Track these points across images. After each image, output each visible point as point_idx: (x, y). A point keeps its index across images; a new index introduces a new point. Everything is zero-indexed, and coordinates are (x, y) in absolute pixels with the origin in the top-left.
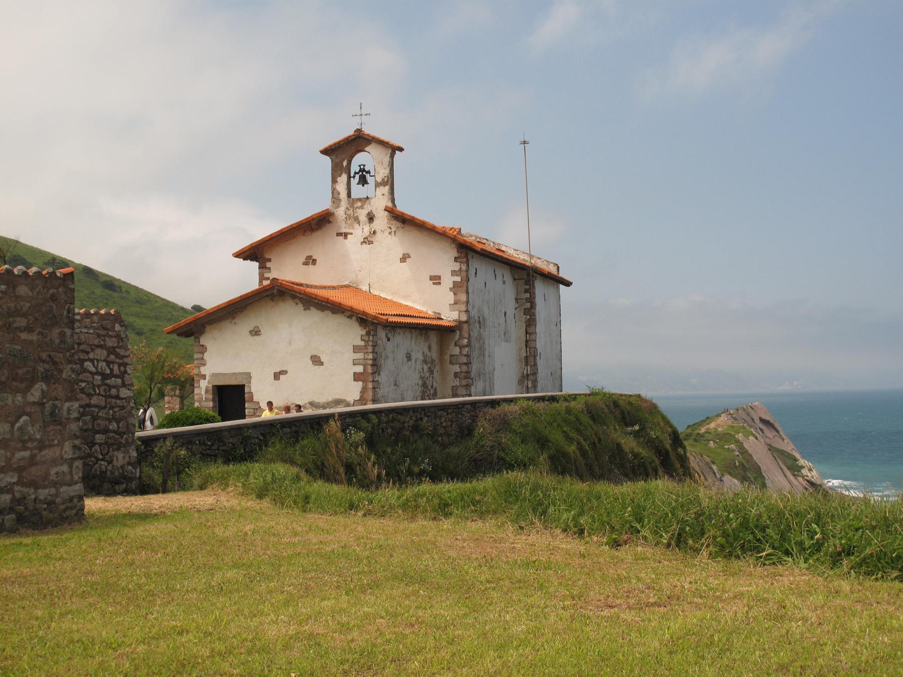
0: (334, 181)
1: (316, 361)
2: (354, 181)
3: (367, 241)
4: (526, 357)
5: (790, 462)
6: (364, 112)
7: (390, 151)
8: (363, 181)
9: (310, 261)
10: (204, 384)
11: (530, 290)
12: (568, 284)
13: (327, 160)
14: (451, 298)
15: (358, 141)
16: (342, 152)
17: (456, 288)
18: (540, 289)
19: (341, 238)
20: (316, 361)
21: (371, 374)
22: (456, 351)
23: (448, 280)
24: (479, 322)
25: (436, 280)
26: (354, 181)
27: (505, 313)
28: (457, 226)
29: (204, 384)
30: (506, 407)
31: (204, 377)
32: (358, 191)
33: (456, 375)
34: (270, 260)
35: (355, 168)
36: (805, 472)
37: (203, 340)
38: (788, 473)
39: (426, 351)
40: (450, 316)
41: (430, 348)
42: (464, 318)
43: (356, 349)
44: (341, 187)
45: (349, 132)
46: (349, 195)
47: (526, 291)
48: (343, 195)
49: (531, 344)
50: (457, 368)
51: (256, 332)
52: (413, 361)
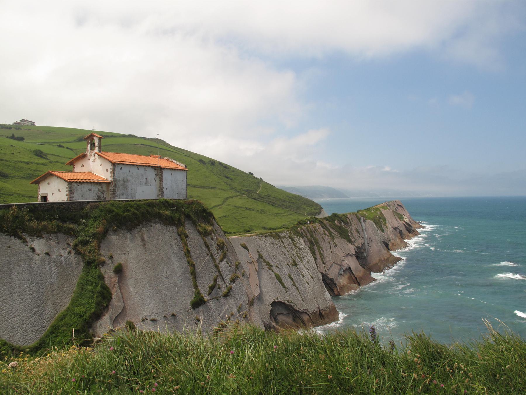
1: (59, 191)
3: (94, 161)
5: (400, 216)
9: (83, 166)
10: (40, 196)
13: (11, 135)
14: (110, 175)
17: (111, 172)
20: (59, 191)
21: (71, 192)
22: (111, 188)
23: (110, 170)
25: (107, 170)
29: (40, 196)
30: (131, 203)
36: (404, 219)
37: (40, 186)
40: (110, 179)
43: (67, 188)
50: (111, 193)
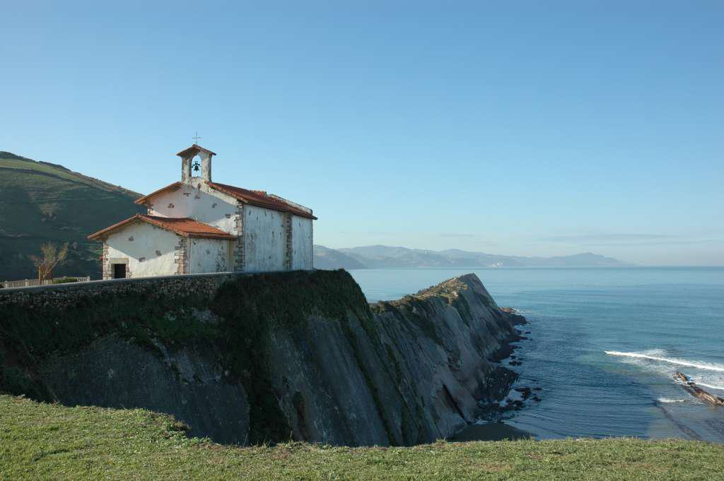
0: (183, 169)
2: (193, 169)
4: (287, 253)
6: (198, 136)
7: (208, 155)
8: (197, 169)
9: (171, 206)
11: (289, 221)
12: (316, 219)
13: (180, 159)
15: (194, 151)
16: (188, 154)
18: (296, 221)
19: (185, 196)
24: (252, 236)
26: (193, 169)
27: (273, 233)
28: (264, 191)
29: (107, 263)
31: (107, 259)
32: (194, 173)
33: (236, 261)
34: (153, 205)
35: (193, 163)
38: (483, 306)
39: (220, 249)
40: (235, 233)
41: (222, 248)
42: (240, 234)
44: (186, 171)
45: (191, 146)
46: (190, 175)
47: (288, 222)
48: (187, 175)
49: (289, 247)
51: (131, 239)
52: (211, 254)
